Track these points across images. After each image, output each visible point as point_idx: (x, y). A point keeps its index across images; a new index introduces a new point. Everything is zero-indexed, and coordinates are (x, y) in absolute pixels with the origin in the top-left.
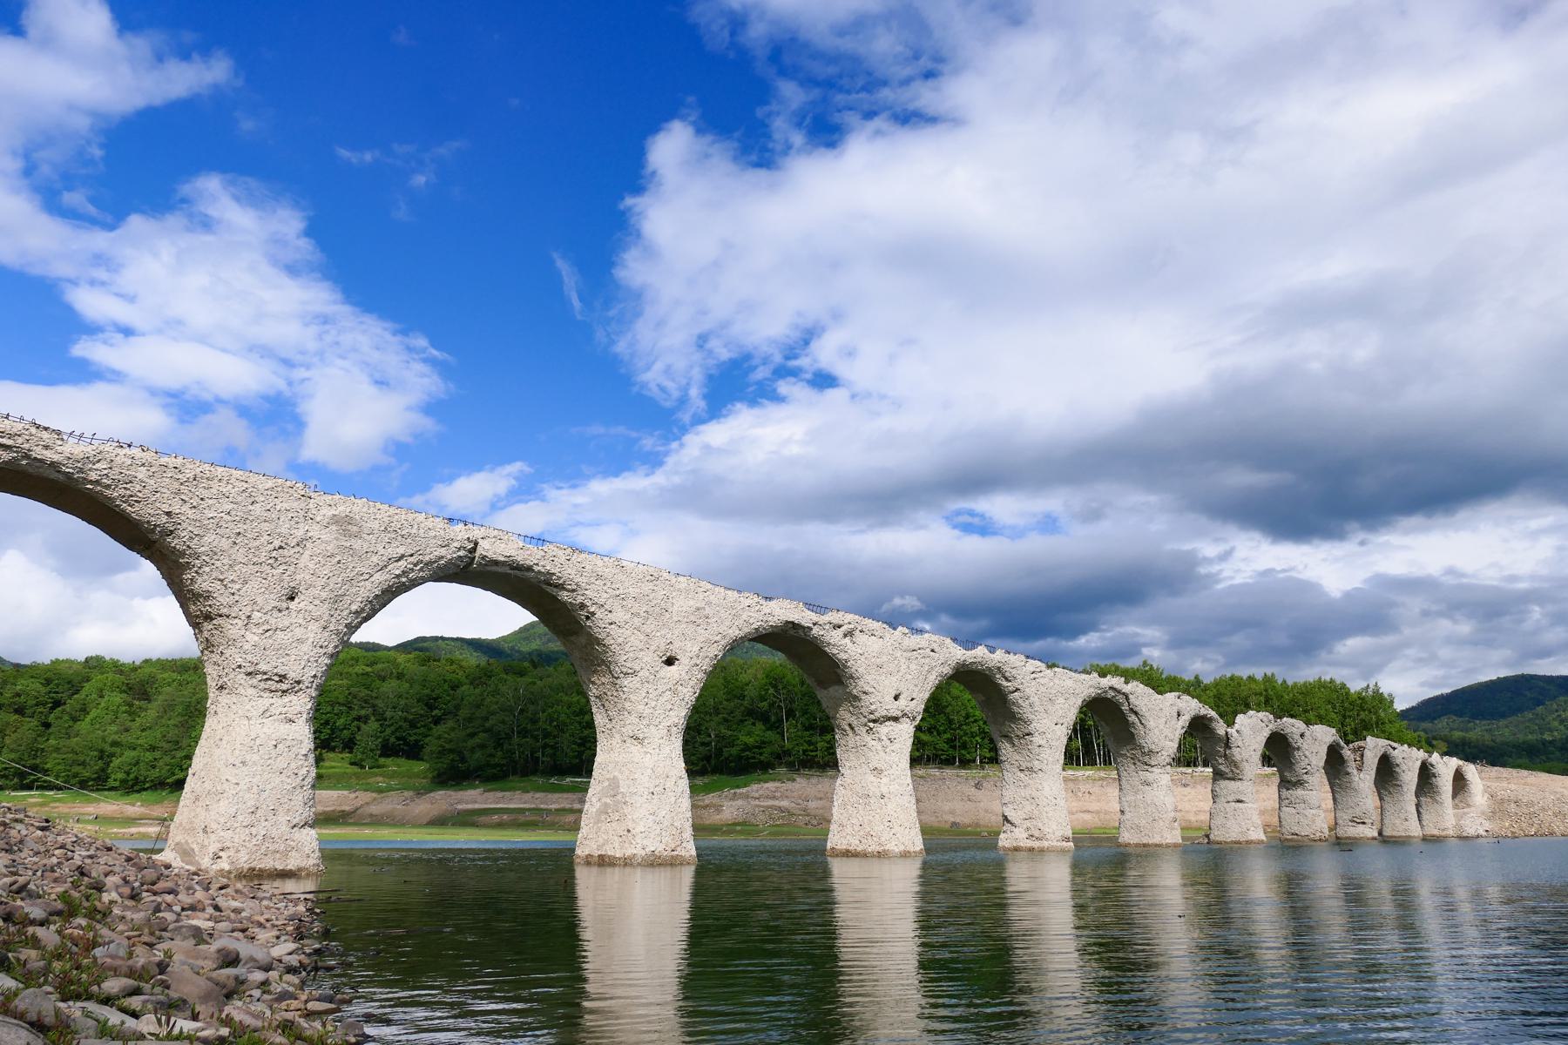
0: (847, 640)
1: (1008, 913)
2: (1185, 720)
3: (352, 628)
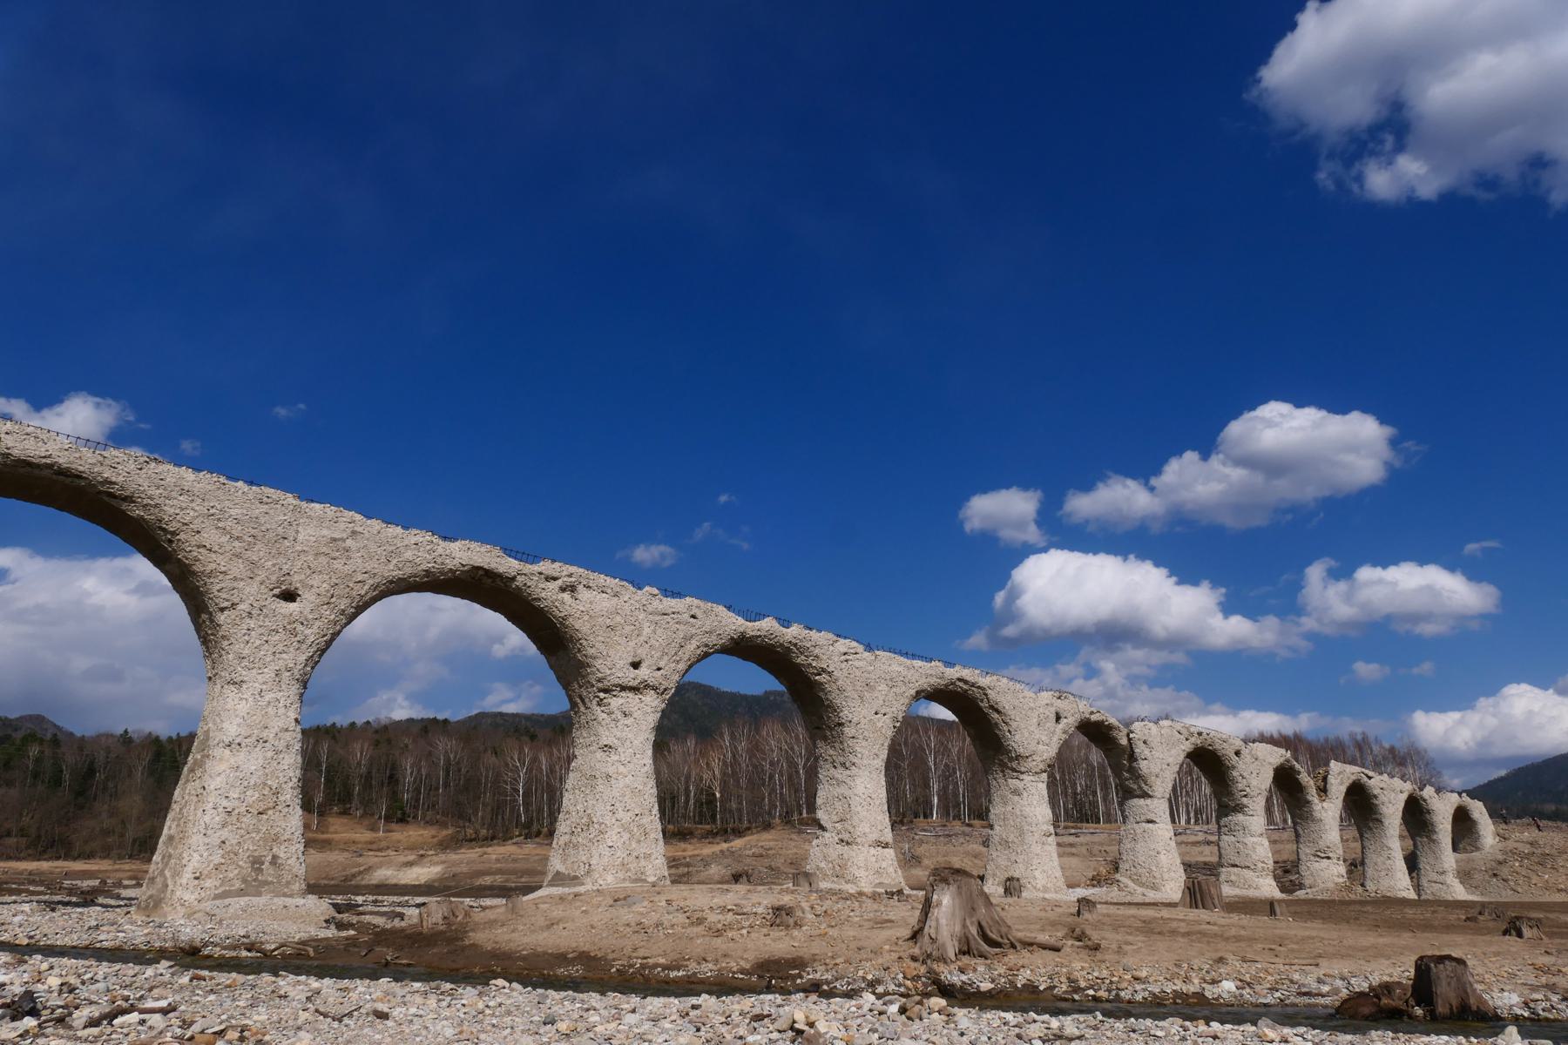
2: (1070, 722)
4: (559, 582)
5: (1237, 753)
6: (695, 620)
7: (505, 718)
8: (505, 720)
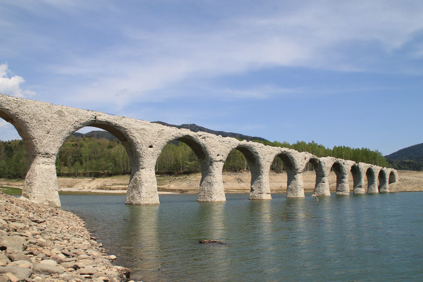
0: (204, 139)
1: (158, 213)
2: (308, 160)
3: (78, 129)
4: (202, 137)
5: (344, 163)
6: (229, 143)
7: (101, 132)
8: (101, 133)
